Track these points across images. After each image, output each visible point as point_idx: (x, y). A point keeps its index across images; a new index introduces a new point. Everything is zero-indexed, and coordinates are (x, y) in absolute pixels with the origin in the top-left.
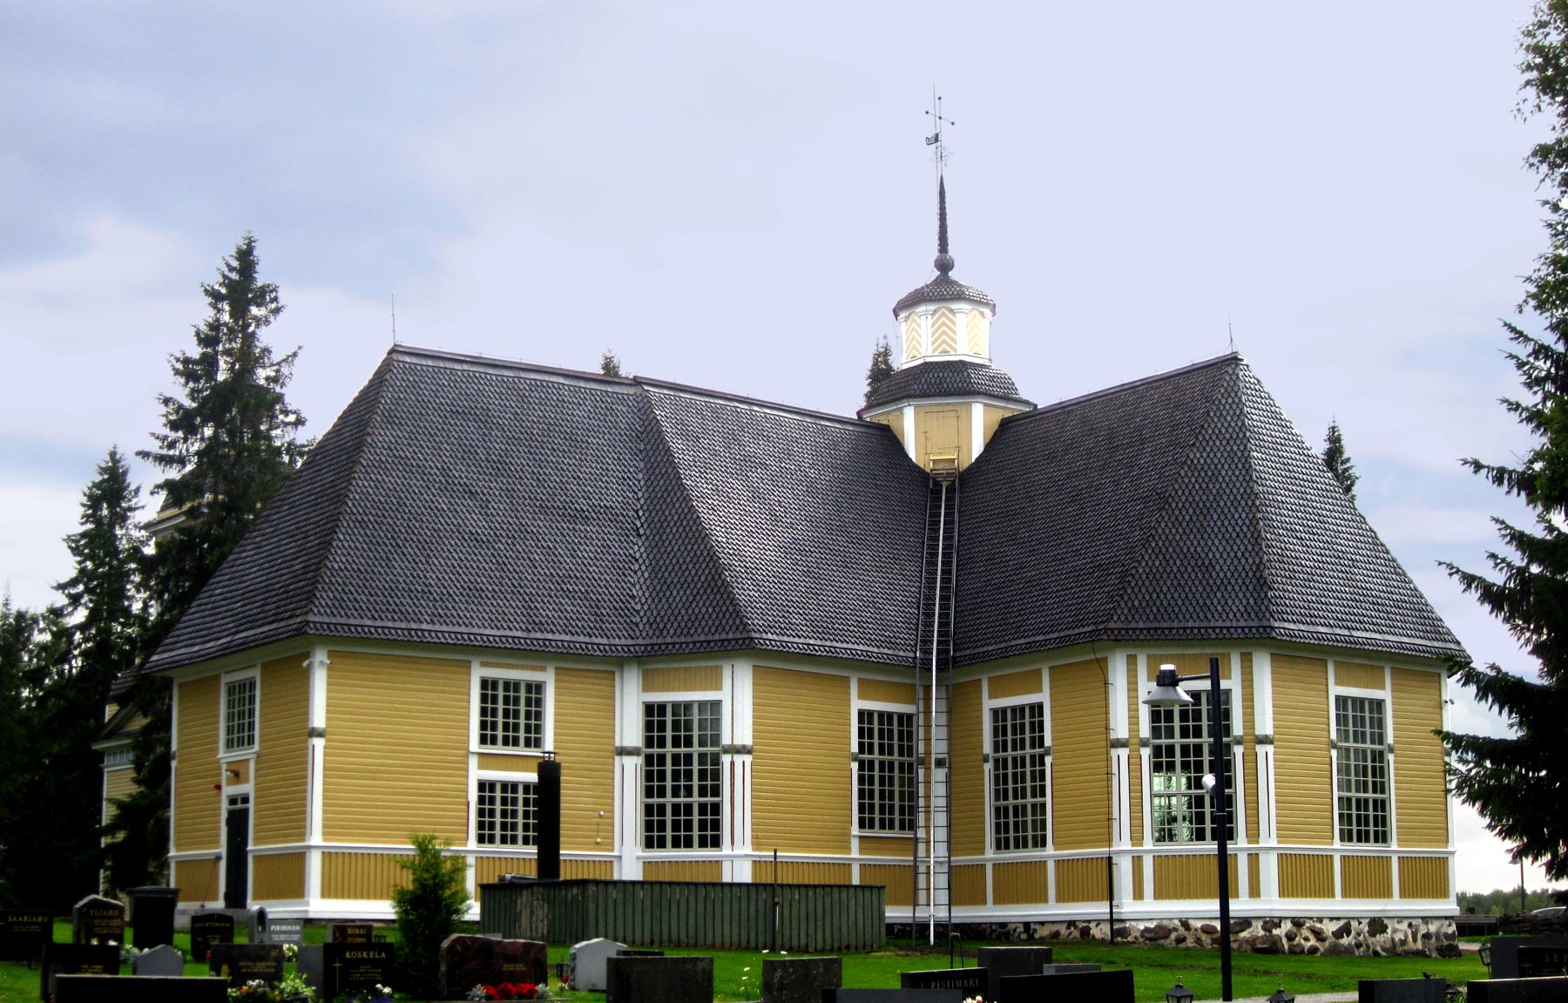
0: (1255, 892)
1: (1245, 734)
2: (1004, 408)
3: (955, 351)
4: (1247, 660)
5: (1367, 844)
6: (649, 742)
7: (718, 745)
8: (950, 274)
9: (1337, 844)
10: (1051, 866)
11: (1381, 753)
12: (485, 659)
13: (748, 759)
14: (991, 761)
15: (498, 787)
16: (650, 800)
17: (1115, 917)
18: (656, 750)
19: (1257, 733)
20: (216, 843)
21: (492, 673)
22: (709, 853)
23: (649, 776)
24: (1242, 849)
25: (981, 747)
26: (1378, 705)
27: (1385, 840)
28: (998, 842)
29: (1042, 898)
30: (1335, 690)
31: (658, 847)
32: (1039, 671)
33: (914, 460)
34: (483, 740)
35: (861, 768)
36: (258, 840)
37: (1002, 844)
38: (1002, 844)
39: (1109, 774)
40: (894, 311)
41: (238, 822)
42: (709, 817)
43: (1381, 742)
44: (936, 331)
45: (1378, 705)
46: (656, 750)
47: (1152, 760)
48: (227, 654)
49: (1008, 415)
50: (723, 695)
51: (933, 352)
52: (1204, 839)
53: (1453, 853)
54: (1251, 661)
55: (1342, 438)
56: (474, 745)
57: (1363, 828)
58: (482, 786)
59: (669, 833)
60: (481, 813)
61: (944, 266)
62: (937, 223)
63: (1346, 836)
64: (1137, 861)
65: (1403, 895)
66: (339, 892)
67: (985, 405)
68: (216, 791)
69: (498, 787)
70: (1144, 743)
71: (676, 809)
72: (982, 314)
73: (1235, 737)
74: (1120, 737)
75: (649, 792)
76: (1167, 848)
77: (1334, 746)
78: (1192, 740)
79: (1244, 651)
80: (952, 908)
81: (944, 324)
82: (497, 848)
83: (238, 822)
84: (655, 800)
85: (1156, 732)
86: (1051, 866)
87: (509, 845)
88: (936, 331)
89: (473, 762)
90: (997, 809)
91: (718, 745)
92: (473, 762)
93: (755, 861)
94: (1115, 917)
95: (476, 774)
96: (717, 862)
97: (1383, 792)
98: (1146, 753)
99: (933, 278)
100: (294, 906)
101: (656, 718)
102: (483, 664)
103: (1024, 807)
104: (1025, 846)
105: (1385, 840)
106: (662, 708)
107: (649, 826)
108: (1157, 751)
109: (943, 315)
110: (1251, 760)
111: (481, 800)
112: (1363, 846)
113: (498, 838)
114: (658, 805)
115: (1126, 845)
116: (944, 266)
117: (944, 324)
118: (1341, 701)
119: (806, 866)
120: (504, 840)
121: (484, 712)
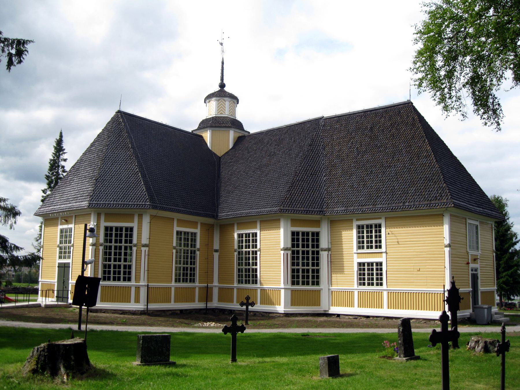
1: (137, 243)
2: (240, 132)
3: (225, 113)
4: (140, 216)
5: (242, 284)
6: (293, 246)
7: (132, 243)
8: (225, 89)
9: (173, 284)
10: (173, 290)
11: (195, 251)
13: (147, 249)
14: (237, 252)
15: (375, 264)
18: (108, 244)
19: (142, 243)
22: (315, 287)
23: (293, 258)
24: (216, 286)
25: (234, 246)
26: (195, 234)
27: (194, 282)
28: (239, 281)
30: (176, 228)
31: (128, 281)
32: (73, 216)
33: (210, 149)
35: (177, 252)
36: (482, 286)
37: (240, 282)
38: (240, 282)
39: (148, 255)
40: (205, 99)
41: (475, 278)
42: (315, 274)
43: (195, 247)
45: (195, 234)
46: (295, 249)
47: (291, 255)
48: (480, 214)
49: (240, 135)
50: (135, 225)
51: (218, 113)
52: (309, 285)
53: (322, 289)
54: (142, 219)
56: (355, 249)
59: (310, 280)
61: (222, 86)
62: (220, 71)
63: (177, 280)
65: (175, 301)
66: (111, 300)
67: (234, 131)
68: (467, 265)
69: (375, 264)
70: (101, 245)
71: (115, 266)
72: (234, 102)
73: (133, 244)
74: (323, 247)
75: (293, 264)
77: (174, 248)
78: (118, 244)
80: (149, 304)
81: (222, 104)
82: (366, 287)
83: (475, 278)
84: (295, 267)
85: (106, 241)
86: (173, 290)
87: (379, 286)
90: (239, 269)
91: (132, 243)
93: (136, 287)
94: (148, 309)
96: (138, 287)
97: (194, 264)
98: (101, 248)
99: (217, 90)
100: (118, 305)
102: (357, 220)
103: (242, 269)
104: (249, 283)
105: (194, 282)
106: (111, 228)
107: (293, 277)
108: (106, 247)
109: (222, 101)
110: (139, 253)
112: (371, 287)
113: (122, 279)
114: (108, 265)
116: (222, 86)
117: (222, 104)
118: (179, 233)
120: (369, 284)
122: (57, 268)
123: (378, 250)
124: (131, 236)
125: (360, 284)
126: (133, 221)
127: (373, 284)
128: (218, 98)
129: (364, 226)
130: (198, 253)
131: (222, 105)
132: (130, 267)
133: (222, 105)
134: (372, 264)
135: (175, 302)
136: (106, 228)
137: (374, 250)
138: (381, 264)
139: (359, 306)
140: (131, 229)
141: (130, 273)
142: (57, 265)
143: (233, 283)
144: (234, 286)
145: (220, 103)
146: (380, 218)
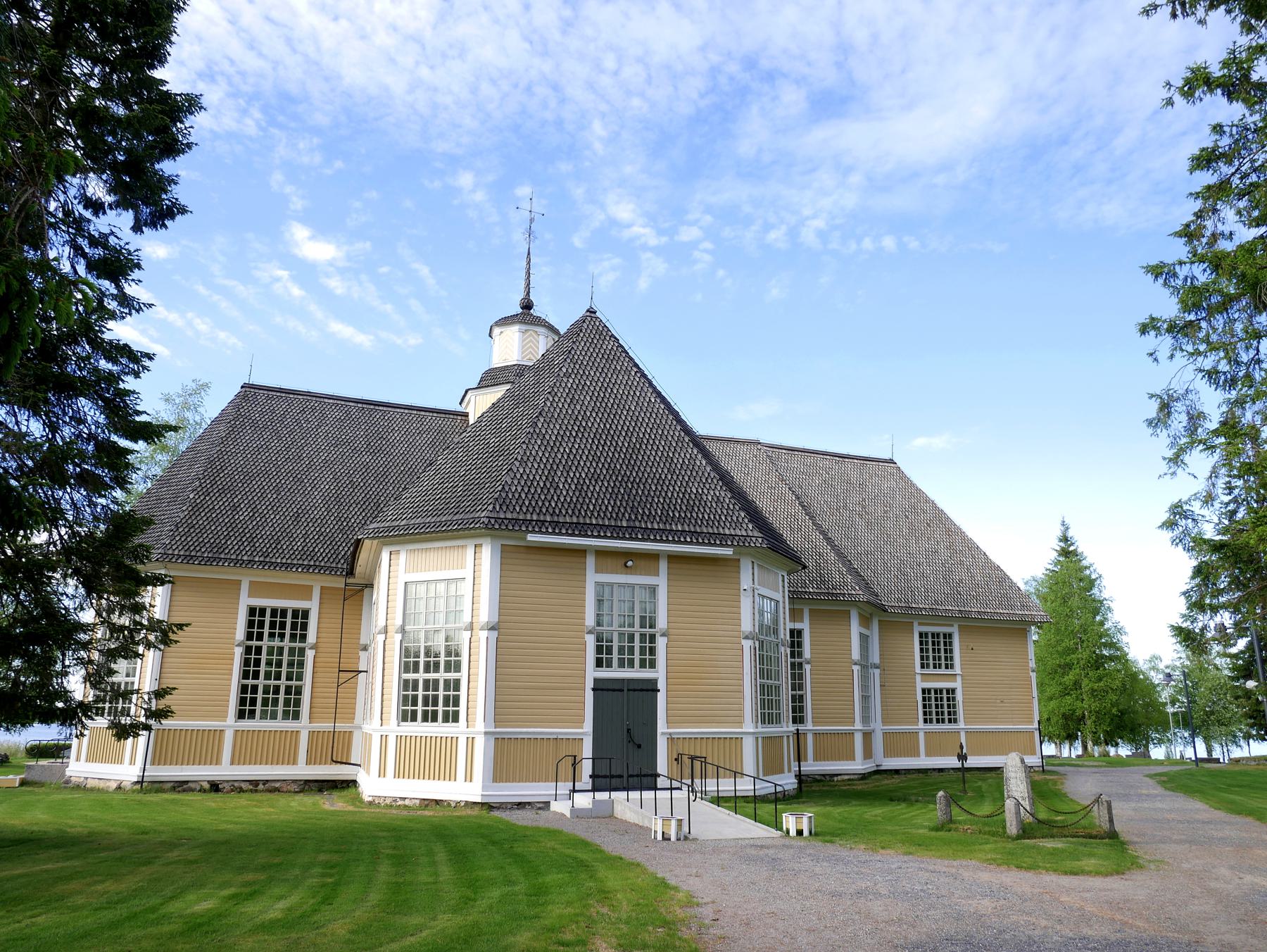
0: (78, 759)
12: (920, 621)
15: (945, 692)
16: (246, 682)
17: (802, 773)
20: (580, 723)
21: (925, 629)
29: (916, 753)
34: (922, 667)
44: (525, 345)
55: (1190, 573)
56: (918, 669)
57: (430, 708)
58: (924, 691)
60: (925, 706)
64: (385, 739)
69: (945, 692)
76: (247, 724)
79: (920, 621)
80: (576, 783)
81: (531, 347)
82: (934, 727)
88: (525, 345)
89: (918, 678)
92: (918, 678)
94: (802, 773)
95: (920, 684)
97: (762, 686)
101: (278, 619)
102: (920, 624)
111: (924, 699)
112: (941, 726)
115: (858, 725)
119: (833, 735)
121: (922, 650)
122: (589, 696)
123: (949, 672)
124: (305, 627)
125: (404, 719)
126: (309, 597)
127: (943, 721)
128: (524, 327)
129: (634, 634)
130: (807, 667)
131: (530, 350)
132: (299, 691)
133: (530, 350)
134: (941, 691)
135: (816, 759)
136: (252, 611)
137: (943, 671)
138: (953, 691)
139: (928, 754)
140: (306, 614)
141: (298, 703)
142: (590, 684)
143: (740, 723)
144: (920, 727)
145: (527, 338)
146: (952, 626)
